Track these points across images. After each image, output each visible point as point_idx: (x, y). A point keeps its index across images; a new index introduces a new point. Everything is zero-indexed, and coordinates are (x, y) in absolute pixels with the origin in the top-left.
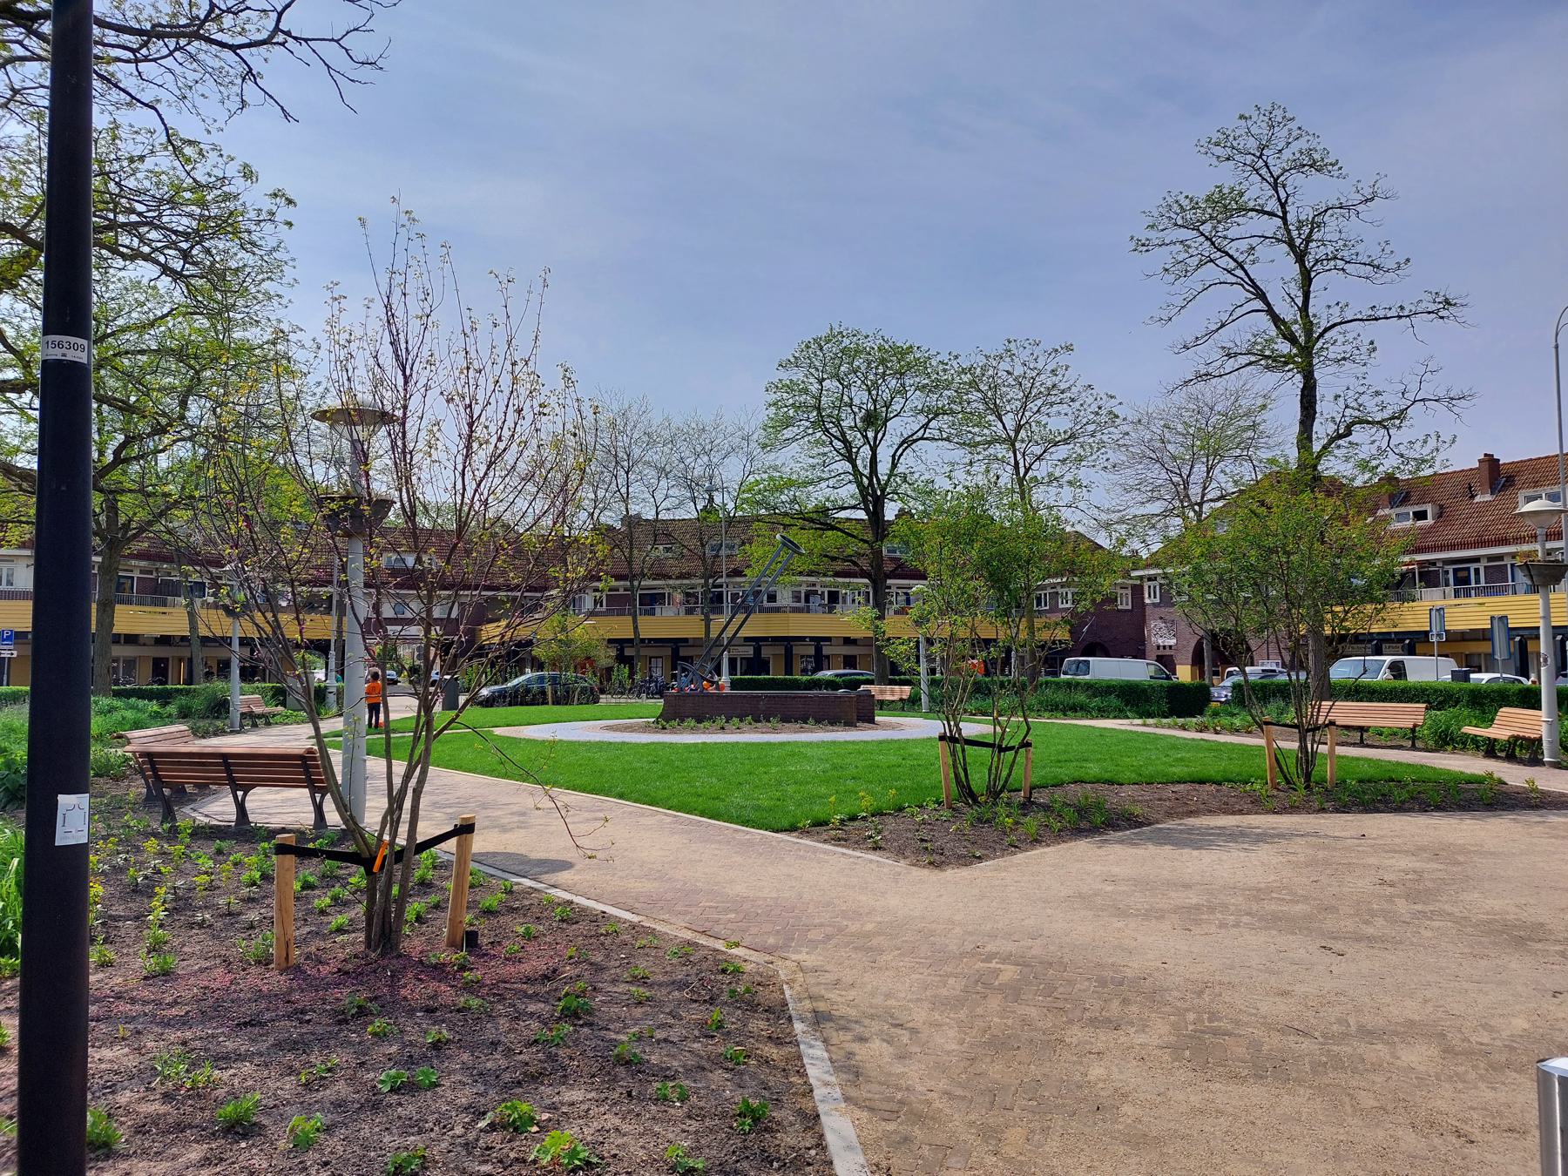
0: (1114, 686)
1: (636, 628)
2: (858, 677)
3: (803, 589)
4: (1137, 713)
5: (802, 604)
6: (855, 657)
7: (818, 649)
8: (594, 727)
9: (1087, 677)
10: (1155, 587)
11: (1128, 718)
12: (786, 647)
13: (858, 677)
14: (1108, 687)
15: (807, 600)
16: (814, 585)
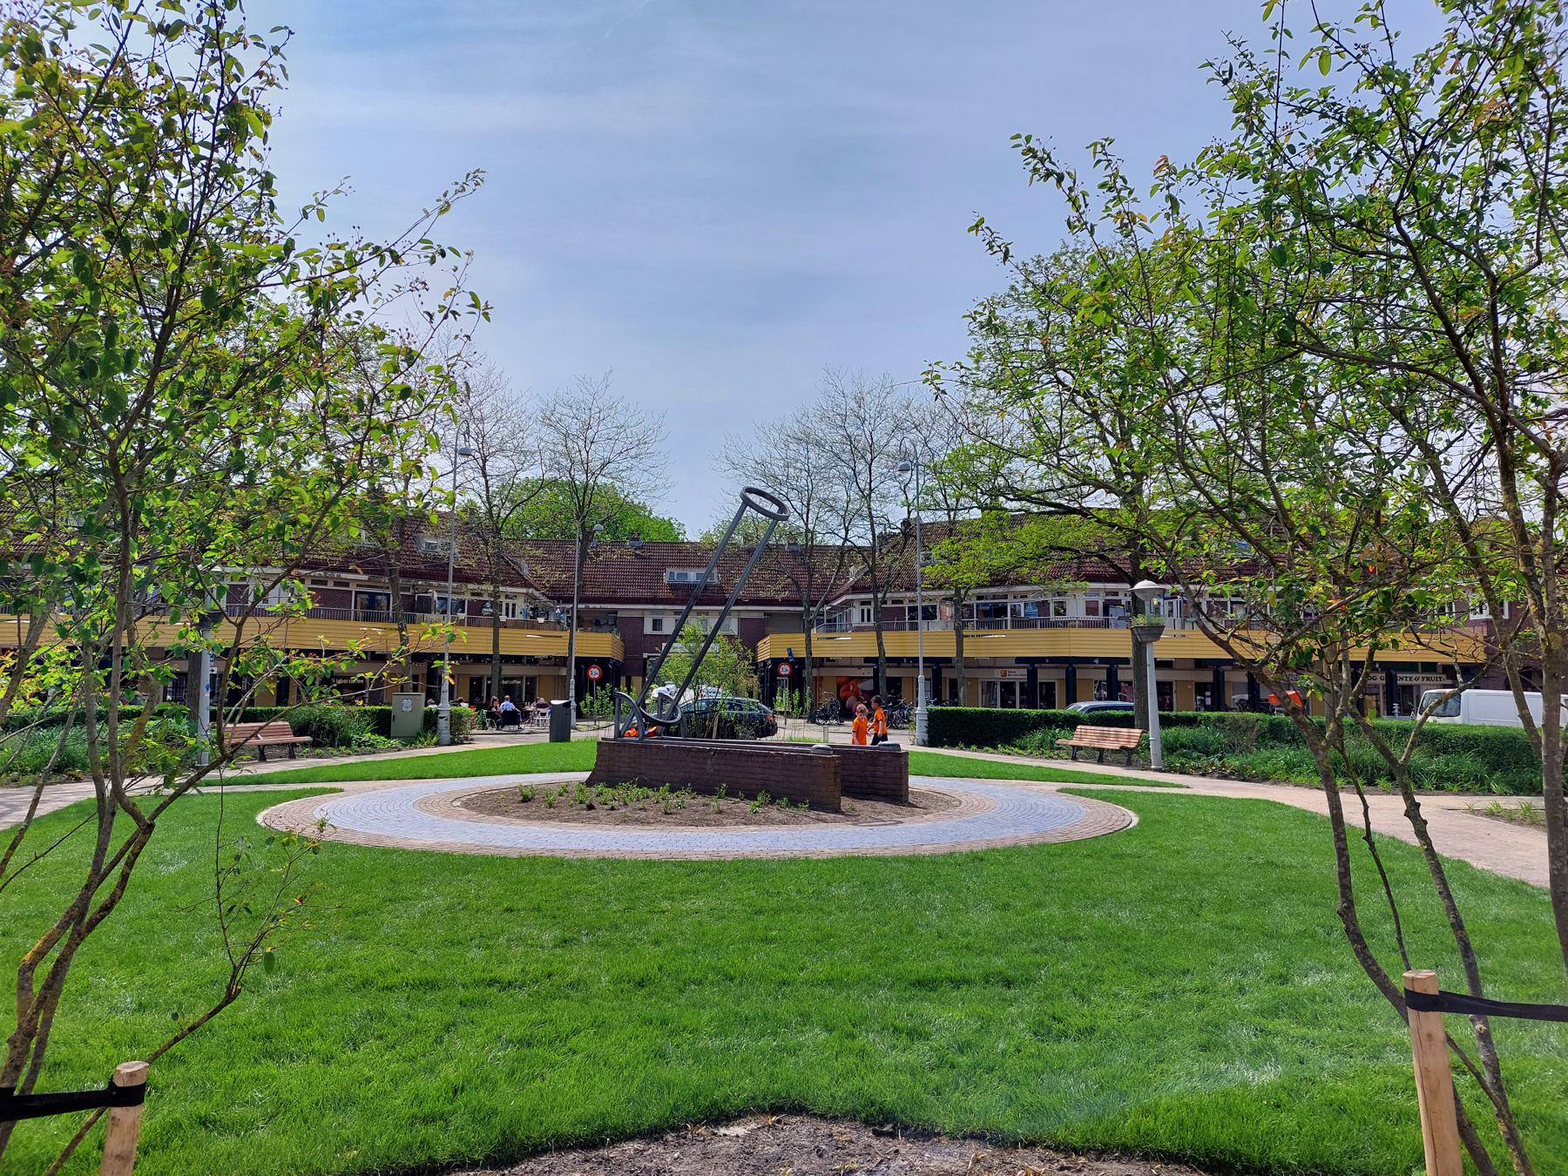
0: (1476, 738)
1: (880, 645)
2: (1111, 712)
3: (1101, 600)
4: (1510, 784)
5: (1100, 617)
6: (1170, 684)
7: (1112, 674)
8: (425, 804)
9: (1458, 720)
10: (869, 611)
11: (1490, 792)
12: (1067, 670)
13: (1111, 712)
14: (1467, 738)
15: (1106, 612)
16: (1116, 594)
